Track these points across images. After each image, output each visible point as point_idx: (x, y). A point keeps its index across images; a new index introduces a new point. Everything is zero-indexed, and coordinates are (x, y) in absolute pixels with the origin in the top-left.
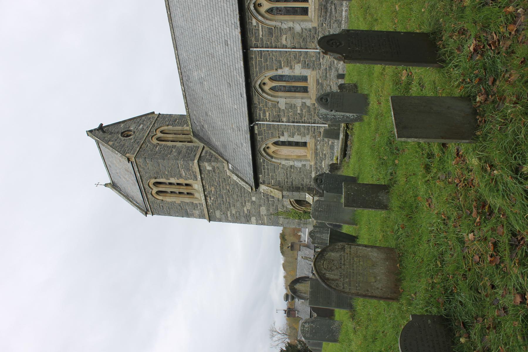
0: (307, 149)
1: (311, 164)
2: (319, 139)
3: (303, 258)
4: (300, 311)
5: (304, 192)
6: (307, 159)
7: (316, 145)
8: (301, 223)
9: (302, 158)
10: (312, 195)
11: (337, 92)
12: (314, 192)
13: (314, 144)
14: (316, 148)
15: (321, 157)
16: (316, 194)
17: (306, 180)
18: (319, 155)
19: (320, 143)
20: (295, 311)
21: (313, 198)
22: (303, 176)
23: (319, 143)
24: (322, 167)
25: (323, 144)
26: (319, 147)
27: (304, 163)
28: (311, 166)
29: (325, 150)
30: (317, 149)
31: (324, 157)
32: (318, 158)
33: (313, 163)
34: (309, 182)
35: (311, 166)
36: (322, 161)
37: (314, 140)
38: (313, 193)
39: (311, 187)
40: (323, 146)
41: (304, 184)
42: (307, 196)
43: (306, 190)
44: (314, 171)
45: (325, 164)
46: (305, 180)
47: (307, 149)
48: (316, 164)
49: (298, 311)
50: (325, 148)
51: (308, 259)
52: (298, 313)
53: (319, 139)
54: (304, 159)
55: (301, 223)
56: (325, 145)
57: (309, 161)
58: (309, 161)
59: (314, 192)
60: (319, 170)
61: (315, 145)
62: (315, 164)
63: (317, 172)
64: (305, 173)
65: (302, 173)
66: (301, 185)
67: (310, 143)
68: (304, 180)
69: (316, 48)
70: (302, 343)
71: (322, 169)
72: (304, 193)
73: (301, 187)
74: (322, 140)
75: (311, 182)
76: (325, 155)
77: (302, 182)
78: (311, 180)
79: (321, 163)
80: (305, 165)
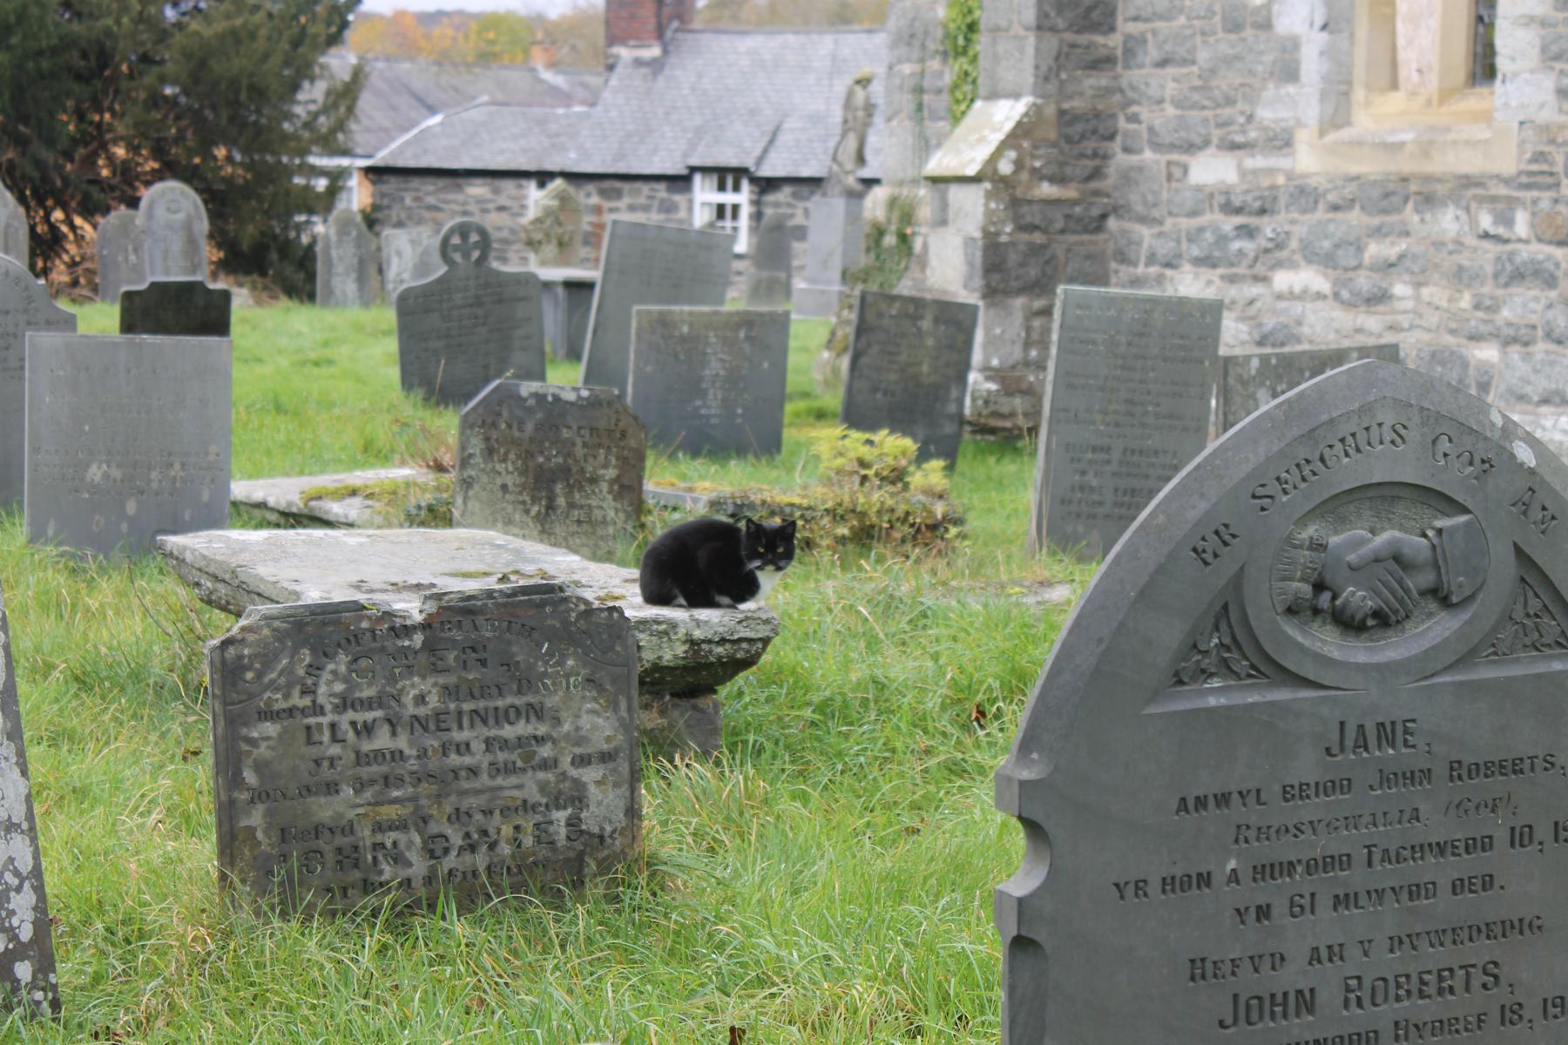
0: (1445, 95)
1: (1303, 138)
2: (1522, 224)
3: (860, 94)
4: (661, 82)
5: (1046, 76)
6: (1359, 94)
7: (1467, 186)
8: (922, 61)
9: (1362, 30)
10: (1005, 167)
11: (658, 456)
12: (1047, 189)
13: (1471, 163)
14: (1441, 189)
15: (1360, 250)
16: (1015, 203)
17: (1171, 89)
18: (1378, 232)
19: (1486, 236)
20: (660, 33)
21: (976, 179)
22: (1203, 56)
23: (1486, 221)
24: (1279, 265)
25: (1477, 277)
26: (1448, 222)
27: (1311, 64)
28: (1282, 141)
29: (1425, 292)
30: (1428, 200)
31: (1364, 282)
32: (1355, 217)
33: (1307, 160)
34: (1151, 129)
35: (1282, 141)
36: (1327, 261)
37: (1509, 167)
38: (1039, 176)
39: (1116, 146)
40: (1460, 277)
41: (1132, 76)
42: (1006, 114)
43: (1063, 94)
44: (1243, 173)
45: (1304, 295)
46: (1167, 83)
47: (1445, 95)
48: (1304, 195)
49: (656, 66)
50: (1435, 293)
51: (852, 143)
52: (639, 63)
53: (1522, 224)
54: (1360, 53)
55: (922, 61)
56: (1466, 301)
57: (1336, 117)
58: (1336, 117)
59: (1047, 189)
60: (1248, 232)
61: (1468, 182)
62: (1302, 190)
63: (1238, 211)
64: (1226, 81)
65: (1225, 44)
66: (1128, 38)
67: (1487, 117)
68: (1171, 71)
69: (392, 184)
70: (342, 110)
71: (1260, 269)
72: (1029, 78)
73: (1115, 41)
74: (1511, 256)
75: (1157, 146)
76: (1378, 298)
77: (1153, 52)
78: (1173, 147)
79: (1311, 255)
80: (1289, 73)
